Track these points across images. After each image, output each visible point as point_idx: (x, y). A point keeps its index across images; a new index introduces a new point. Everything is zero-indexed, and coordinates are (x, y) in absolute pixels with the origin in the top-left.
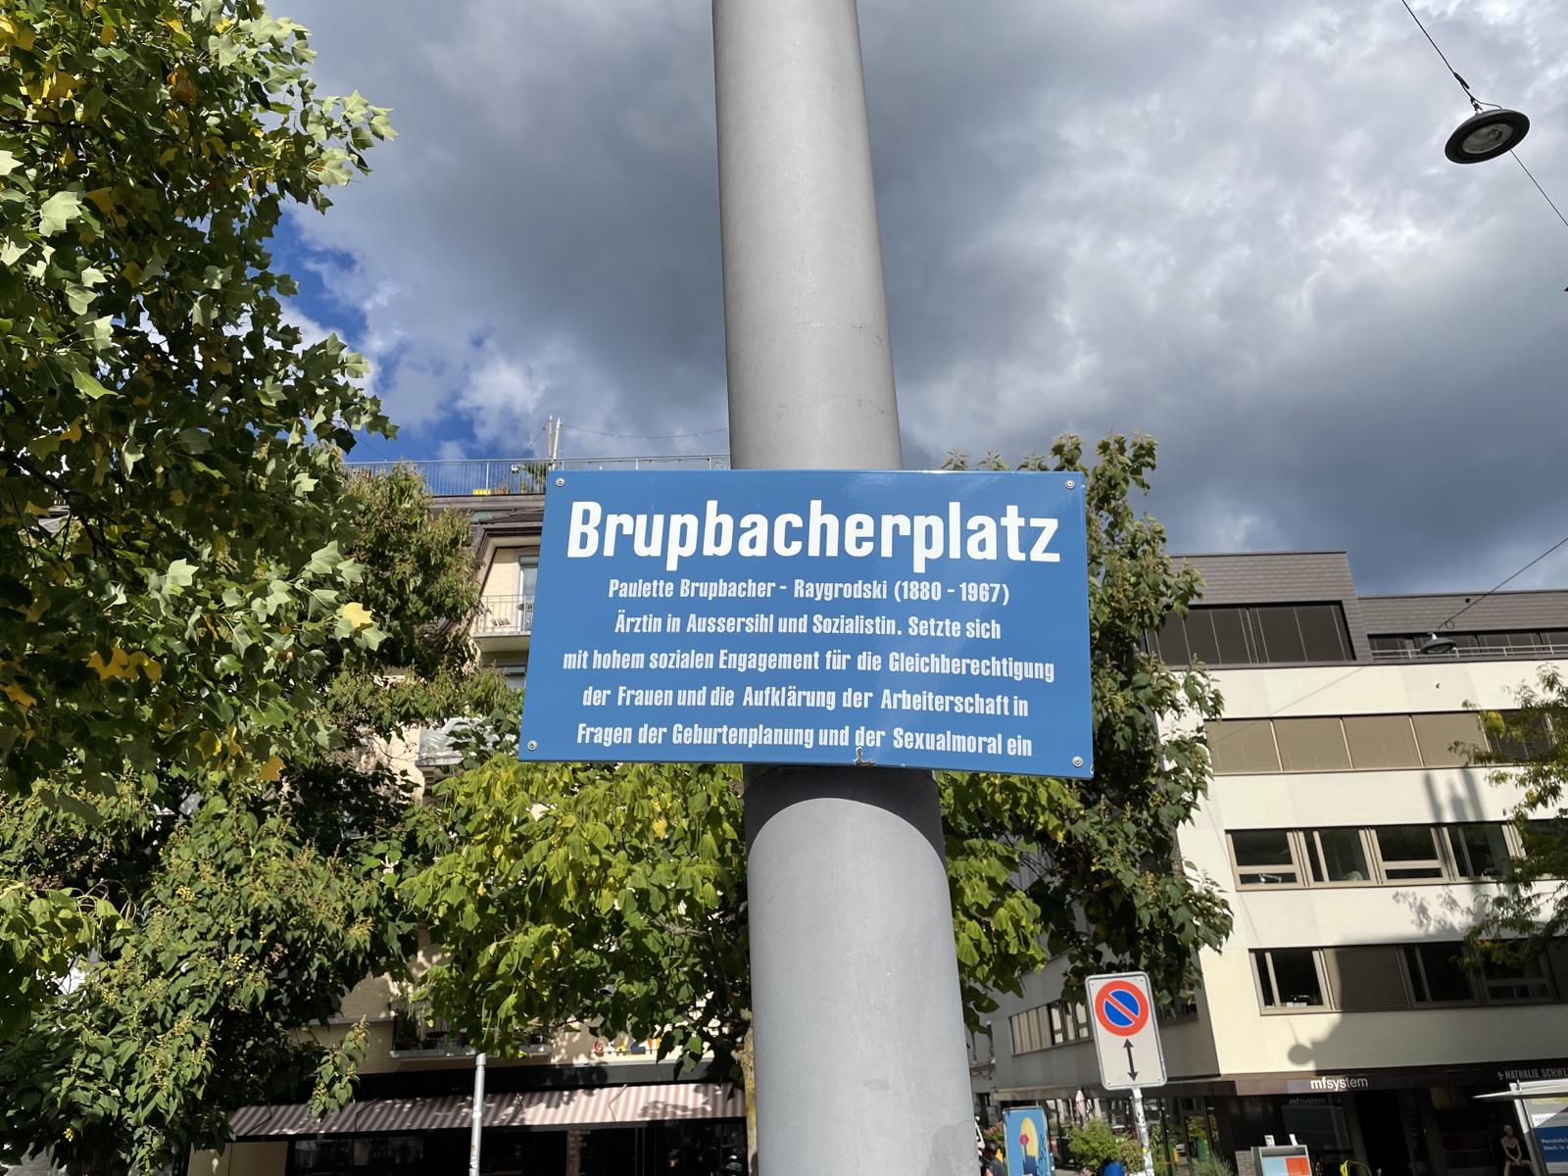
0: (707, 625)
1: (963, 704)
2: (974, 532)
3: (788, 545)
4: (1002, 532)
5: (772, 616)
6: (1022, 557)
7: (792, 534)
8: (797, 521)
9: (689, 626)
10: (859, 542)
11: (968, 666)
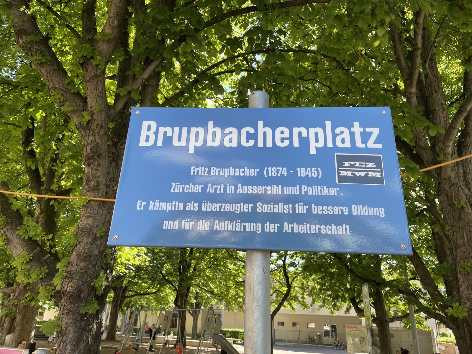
0: (248, 190)
1: (326, 229)
2: (338, 135)
3: (247, 141)
4: (352, 135)
5: (280, 186)
6: (363, 146)
7: (249, 136)
8: (252, 131)
9: (238, 190)
10: (282, 140)
11: (342, 210)
